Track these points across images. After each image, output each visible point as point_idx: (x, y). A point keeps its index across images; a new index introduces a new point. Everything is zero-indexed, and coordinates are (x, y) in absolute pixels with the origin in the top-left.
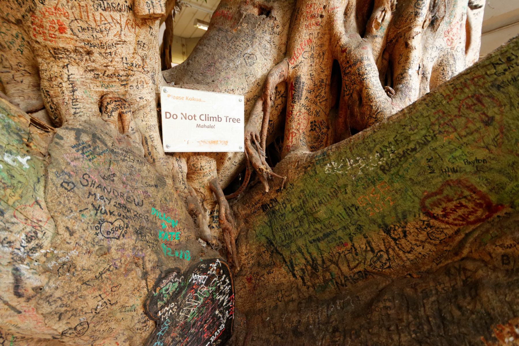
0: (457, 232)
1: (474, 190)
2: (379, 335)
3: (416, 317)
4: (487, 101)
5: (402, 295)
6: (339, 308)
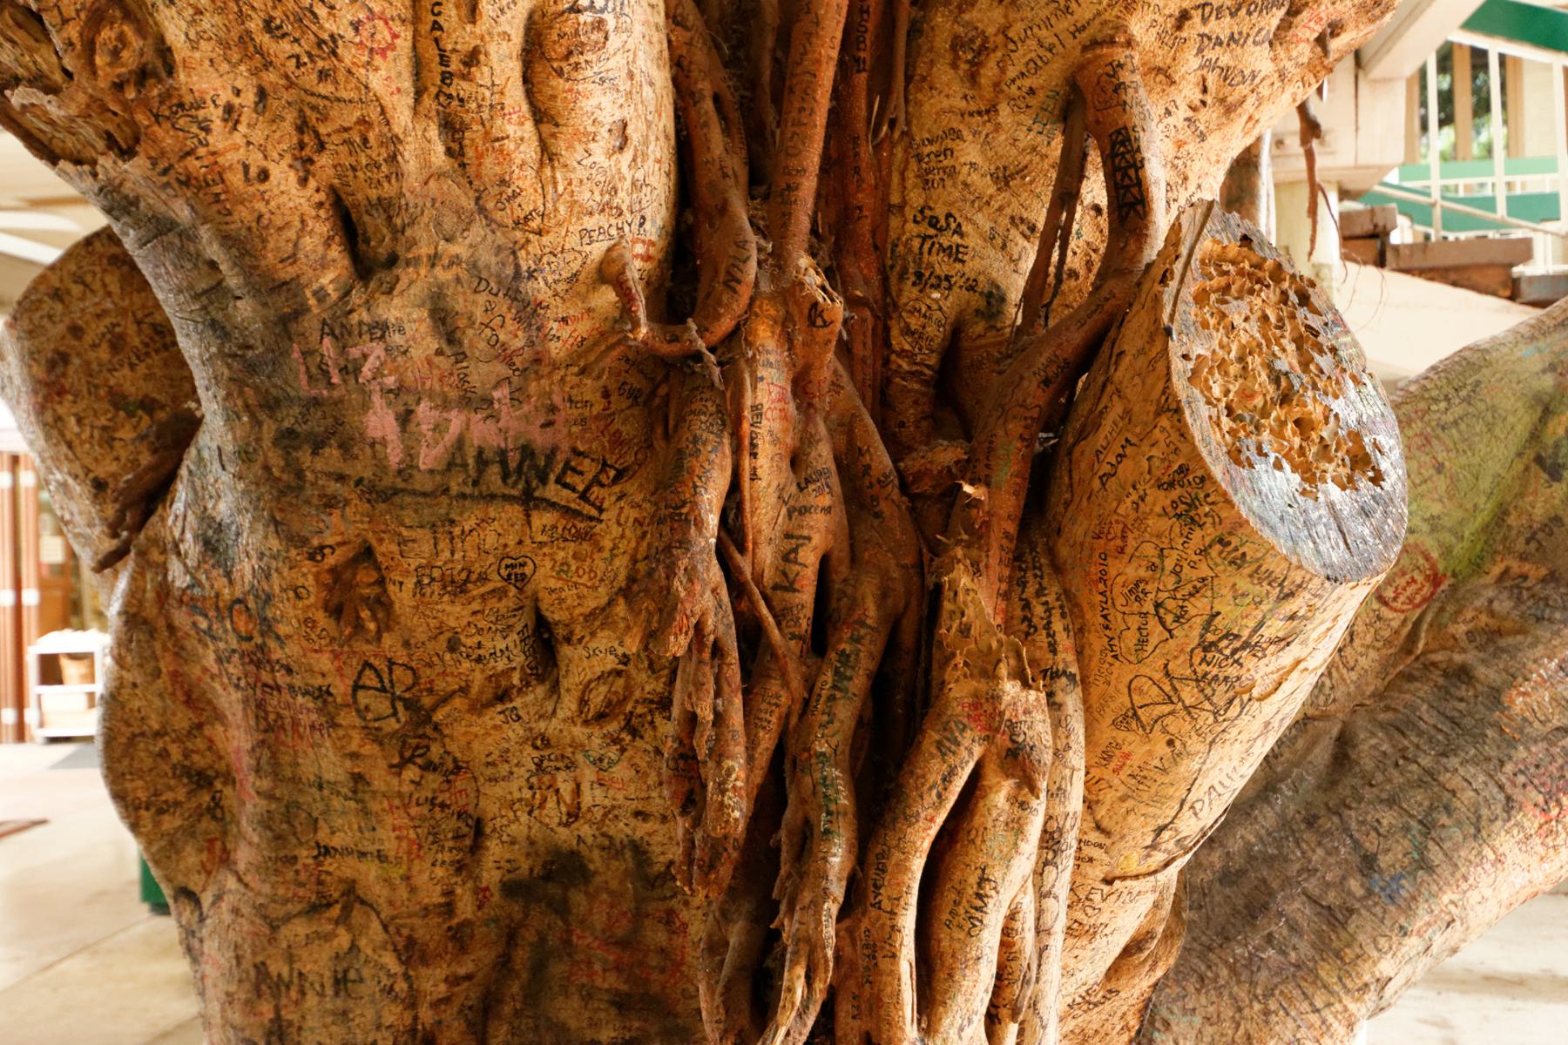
0: (1404, 622)
1: (1427, 558)
2: (1390, 781)
3: (1421, 734)
4: (1435, 442)
5: (1382, 726)
6: (1290, 793)
